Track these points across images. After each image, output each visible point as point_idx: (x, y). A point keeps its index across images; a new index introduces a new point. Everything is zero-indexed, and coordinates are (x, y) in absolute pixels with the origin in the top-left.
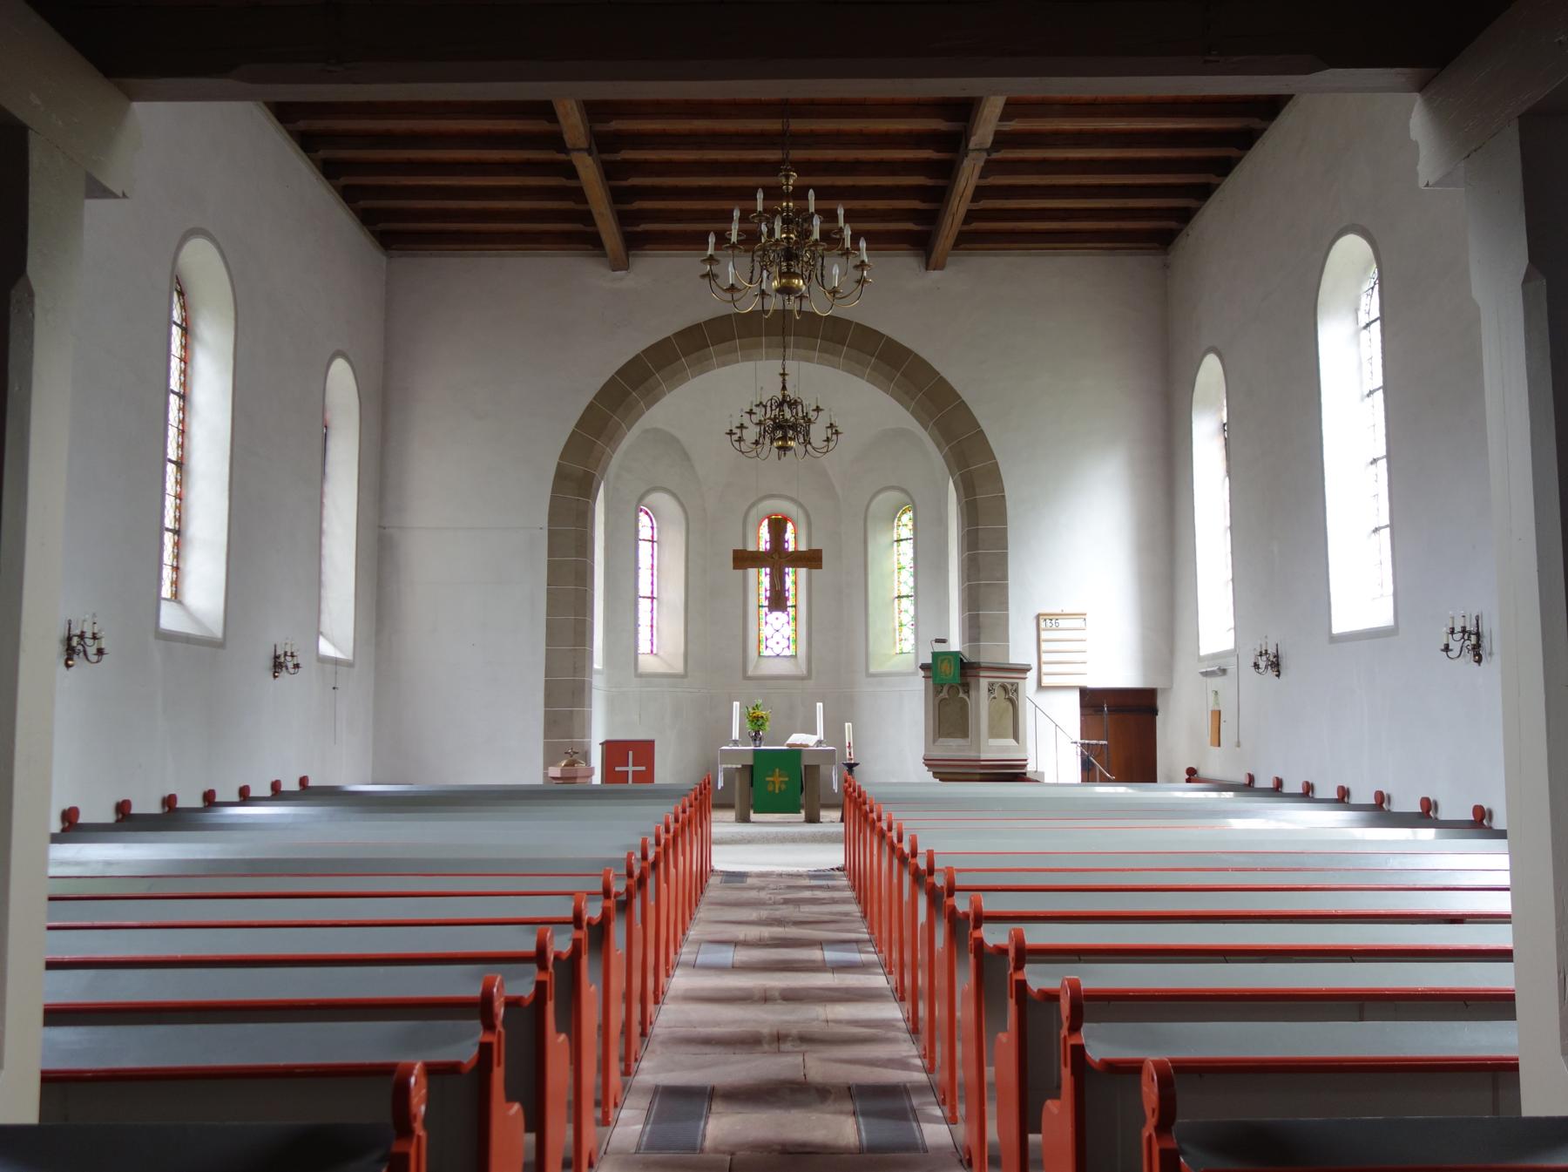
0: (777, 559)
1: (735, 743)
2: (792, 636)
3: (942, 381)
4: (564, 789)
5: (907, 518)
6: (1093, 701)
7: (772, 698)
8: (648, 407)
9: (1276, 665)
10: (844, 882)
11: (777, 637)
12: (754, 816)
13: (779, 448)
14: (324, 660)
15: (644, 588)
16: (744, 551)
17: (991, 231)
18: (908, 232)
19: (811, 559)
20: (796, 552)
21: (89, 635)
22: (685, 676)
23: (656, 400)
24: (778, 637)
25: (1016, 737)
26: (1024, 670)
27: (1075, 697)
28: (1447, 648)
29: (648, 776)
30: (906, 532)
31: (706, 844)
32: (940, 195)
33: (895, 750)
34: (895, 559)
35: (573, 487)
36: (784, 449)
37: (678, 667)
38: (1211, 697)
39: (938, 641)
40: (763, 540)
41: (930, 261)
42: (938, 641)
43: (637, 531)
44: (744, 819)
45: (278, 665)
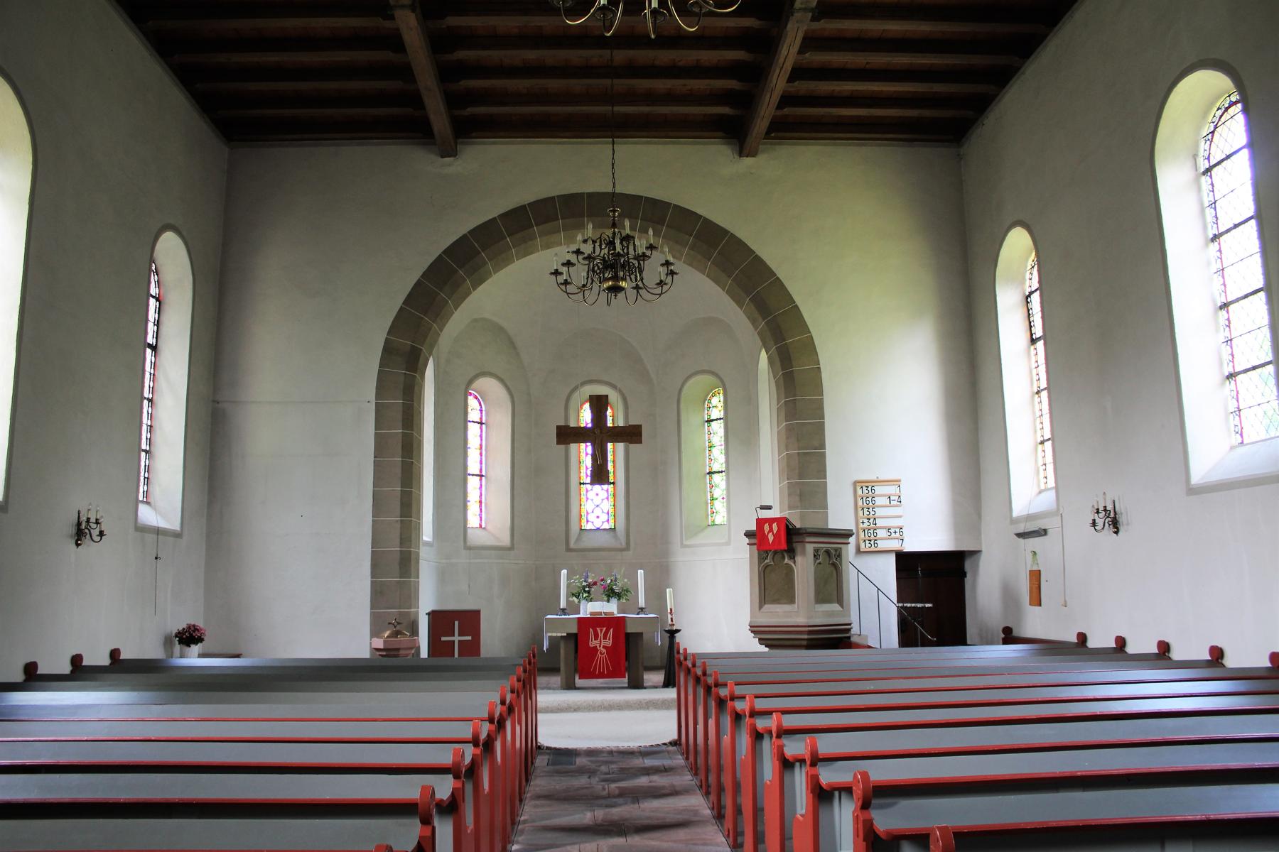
0: (599, 435)
1: (564, 611)
2: (611, 511)
3: (758, 260)
4: (388, 666)
5: (717, 401)
6: (908, 563)
7: (598, 566)
8: (475, 287)
9: (1115, 524)
10: (679, 760)
11: (597, 508)
12: (579, 682)
13: (610, 289)
14: (143, 529)
15: (473, 467)
16: (567, 427)
17: (796, 124)
18: (722, 117)
19: (630, 434)
20: (613, 428)
21: (93, 520)
22: (511, 548)
23: (482, 281)
24: (598, 512)
25: (840, 601)
26: (847, 534)
27: (891, 561)
28: (1094, 524)
29: (472, 648)
30: (717, 413)
31: (531, 711)
32: (756, 74)
33: (717, 610)
34: (709, 436)
35: (403, 358)
36: (616, 289)
37: (505, 539)
38: (1030, 556)
39: (762, 508)
40: (585, 417)
41: (742, 152)
42: (762, 508)
43: (466, 413)
44: (570, 686)
45: (80, 533)
